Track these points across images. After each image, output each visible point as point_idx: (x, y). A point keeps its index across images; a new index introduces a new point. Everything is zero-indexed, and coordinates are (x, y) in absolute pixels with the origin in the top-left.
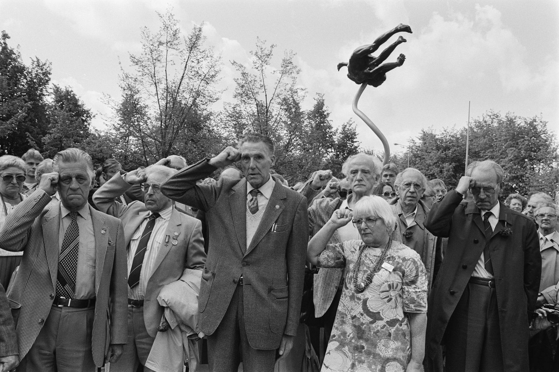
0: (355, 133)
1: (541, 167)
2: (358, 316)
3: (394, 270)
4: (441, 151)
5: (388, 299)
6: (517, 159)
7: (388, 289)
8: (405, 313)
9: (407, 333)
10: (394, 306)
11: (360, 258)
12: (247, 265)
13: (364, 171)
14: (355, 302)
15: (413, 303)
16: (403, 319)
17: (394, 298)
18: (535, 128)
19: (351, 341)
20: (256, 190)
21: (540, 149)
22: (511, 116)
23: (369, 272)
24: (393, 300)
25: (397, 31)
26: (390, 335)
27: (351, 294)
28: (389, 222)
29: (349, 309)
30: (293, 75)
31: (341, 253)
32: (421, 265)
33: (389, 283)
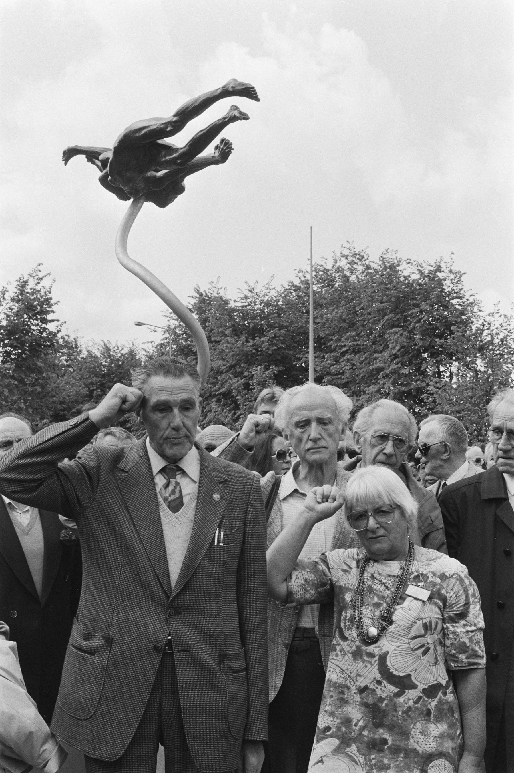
1: (454, 370)
2: (372, 687)
3: (430, 598)
4: (243, 338)
5: (424, 649)
6: (406, 352)
7: (423, 632)
8: (449, 671)
9: (455, 707)
10: (433, 661)
11: (361, 582)
12: (175, 614)
14: (364, 661)
15: (465, 652)
16: (447, 682)
17: (432, 647)
18: (440, 283)
19: (360, 734)
20: (172, 466)
21: (452, 333)
22: (392, 257)
23: (385, 605)
24: (432, 651)
25: (225, 93)
26: (429, 713)
27: (354, 648)
28: (412, 512)
29: (353, 675)
31: (325, 575)
32: (471, 584)
33: (424, 621)
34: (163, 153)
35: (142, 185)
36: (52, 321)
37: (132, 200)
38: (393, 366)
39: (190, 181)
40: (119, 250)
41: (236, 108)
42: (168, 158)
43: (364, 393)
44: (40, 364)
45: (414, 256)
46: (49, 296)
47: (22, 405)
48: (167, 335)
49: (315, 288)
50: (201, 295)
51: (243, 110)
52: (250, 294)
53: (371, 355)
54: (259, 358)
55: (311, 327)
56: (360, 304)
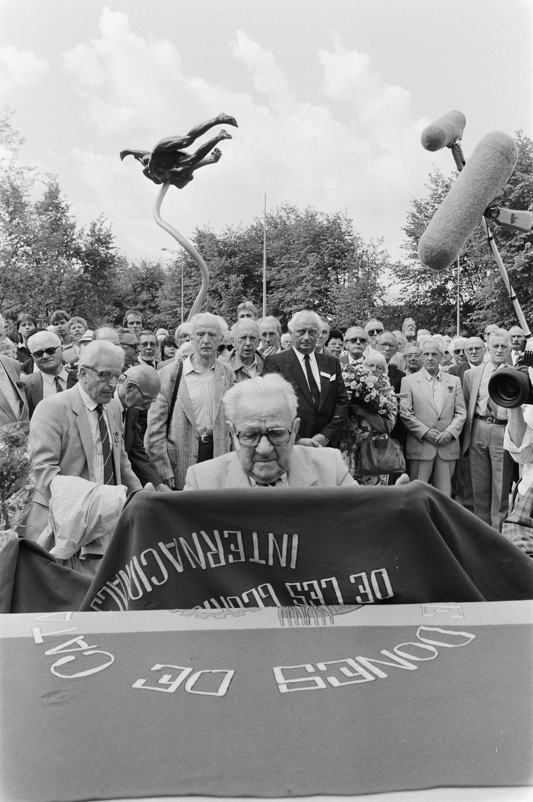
0: (109, 235)
4: (224, 258)
13: (210, 334)
21: (345, 256)
22: (312, 210)
25: (218, 122)
30: (13, 146)
34: (181, 158)
35: (168, 177)
36: (112, 248)
37: (162, 184)
38: (312, 275)
39: (196, 173)
40: (156, 214)
41: (224, 131)
42: (184, 161)
43: (295, 291)
44: (105, 273)
45: (325, 210)
46: (110, 233)
47: (96, 299)
48: (180, 256)
49: (267, 229)
50: (200, 232)
51: (228, 133)
52: (228, 232)
53: (298, 269)
54: (234, 270)
55: (264, 251)
56: (292, 238)
